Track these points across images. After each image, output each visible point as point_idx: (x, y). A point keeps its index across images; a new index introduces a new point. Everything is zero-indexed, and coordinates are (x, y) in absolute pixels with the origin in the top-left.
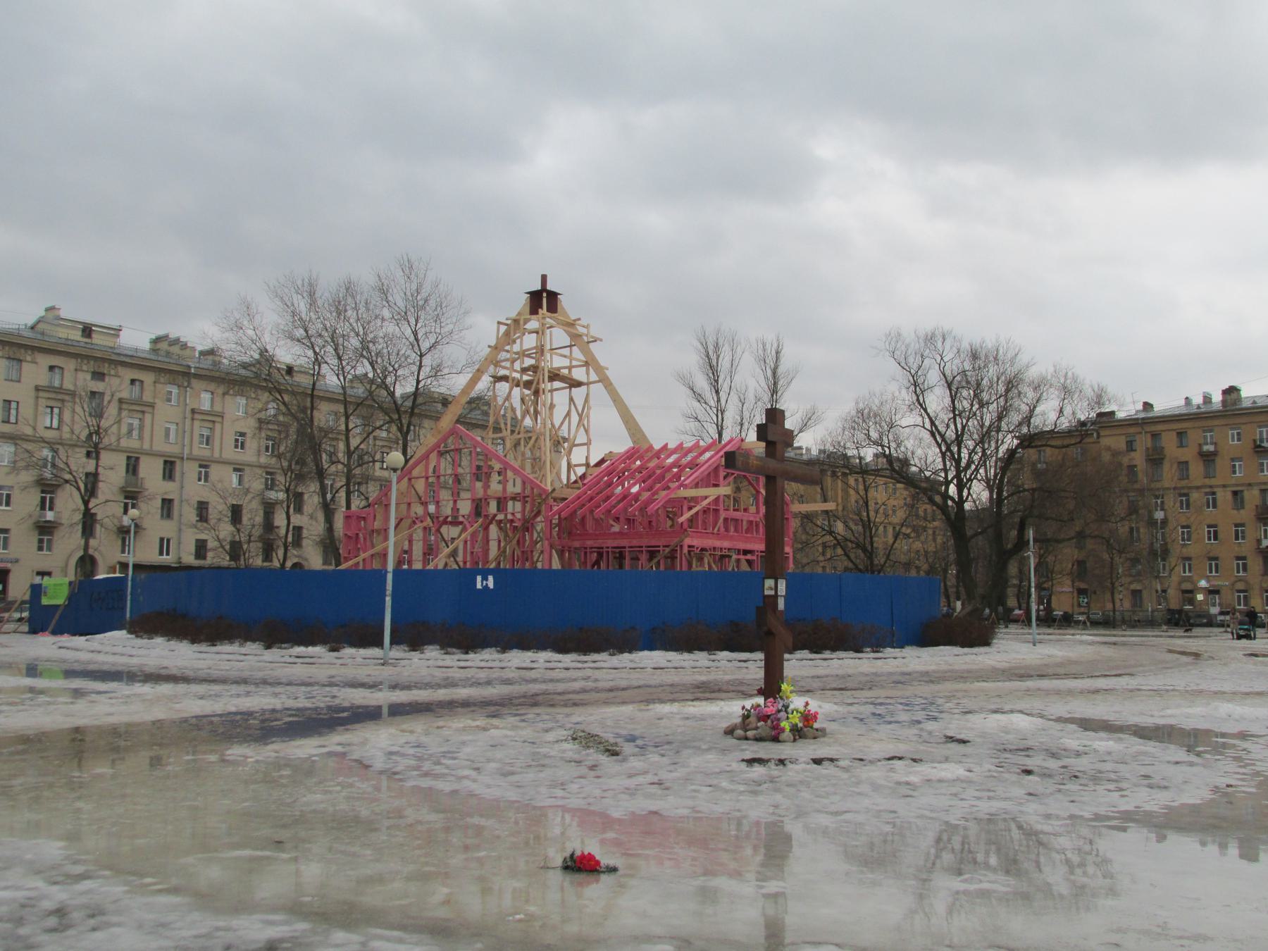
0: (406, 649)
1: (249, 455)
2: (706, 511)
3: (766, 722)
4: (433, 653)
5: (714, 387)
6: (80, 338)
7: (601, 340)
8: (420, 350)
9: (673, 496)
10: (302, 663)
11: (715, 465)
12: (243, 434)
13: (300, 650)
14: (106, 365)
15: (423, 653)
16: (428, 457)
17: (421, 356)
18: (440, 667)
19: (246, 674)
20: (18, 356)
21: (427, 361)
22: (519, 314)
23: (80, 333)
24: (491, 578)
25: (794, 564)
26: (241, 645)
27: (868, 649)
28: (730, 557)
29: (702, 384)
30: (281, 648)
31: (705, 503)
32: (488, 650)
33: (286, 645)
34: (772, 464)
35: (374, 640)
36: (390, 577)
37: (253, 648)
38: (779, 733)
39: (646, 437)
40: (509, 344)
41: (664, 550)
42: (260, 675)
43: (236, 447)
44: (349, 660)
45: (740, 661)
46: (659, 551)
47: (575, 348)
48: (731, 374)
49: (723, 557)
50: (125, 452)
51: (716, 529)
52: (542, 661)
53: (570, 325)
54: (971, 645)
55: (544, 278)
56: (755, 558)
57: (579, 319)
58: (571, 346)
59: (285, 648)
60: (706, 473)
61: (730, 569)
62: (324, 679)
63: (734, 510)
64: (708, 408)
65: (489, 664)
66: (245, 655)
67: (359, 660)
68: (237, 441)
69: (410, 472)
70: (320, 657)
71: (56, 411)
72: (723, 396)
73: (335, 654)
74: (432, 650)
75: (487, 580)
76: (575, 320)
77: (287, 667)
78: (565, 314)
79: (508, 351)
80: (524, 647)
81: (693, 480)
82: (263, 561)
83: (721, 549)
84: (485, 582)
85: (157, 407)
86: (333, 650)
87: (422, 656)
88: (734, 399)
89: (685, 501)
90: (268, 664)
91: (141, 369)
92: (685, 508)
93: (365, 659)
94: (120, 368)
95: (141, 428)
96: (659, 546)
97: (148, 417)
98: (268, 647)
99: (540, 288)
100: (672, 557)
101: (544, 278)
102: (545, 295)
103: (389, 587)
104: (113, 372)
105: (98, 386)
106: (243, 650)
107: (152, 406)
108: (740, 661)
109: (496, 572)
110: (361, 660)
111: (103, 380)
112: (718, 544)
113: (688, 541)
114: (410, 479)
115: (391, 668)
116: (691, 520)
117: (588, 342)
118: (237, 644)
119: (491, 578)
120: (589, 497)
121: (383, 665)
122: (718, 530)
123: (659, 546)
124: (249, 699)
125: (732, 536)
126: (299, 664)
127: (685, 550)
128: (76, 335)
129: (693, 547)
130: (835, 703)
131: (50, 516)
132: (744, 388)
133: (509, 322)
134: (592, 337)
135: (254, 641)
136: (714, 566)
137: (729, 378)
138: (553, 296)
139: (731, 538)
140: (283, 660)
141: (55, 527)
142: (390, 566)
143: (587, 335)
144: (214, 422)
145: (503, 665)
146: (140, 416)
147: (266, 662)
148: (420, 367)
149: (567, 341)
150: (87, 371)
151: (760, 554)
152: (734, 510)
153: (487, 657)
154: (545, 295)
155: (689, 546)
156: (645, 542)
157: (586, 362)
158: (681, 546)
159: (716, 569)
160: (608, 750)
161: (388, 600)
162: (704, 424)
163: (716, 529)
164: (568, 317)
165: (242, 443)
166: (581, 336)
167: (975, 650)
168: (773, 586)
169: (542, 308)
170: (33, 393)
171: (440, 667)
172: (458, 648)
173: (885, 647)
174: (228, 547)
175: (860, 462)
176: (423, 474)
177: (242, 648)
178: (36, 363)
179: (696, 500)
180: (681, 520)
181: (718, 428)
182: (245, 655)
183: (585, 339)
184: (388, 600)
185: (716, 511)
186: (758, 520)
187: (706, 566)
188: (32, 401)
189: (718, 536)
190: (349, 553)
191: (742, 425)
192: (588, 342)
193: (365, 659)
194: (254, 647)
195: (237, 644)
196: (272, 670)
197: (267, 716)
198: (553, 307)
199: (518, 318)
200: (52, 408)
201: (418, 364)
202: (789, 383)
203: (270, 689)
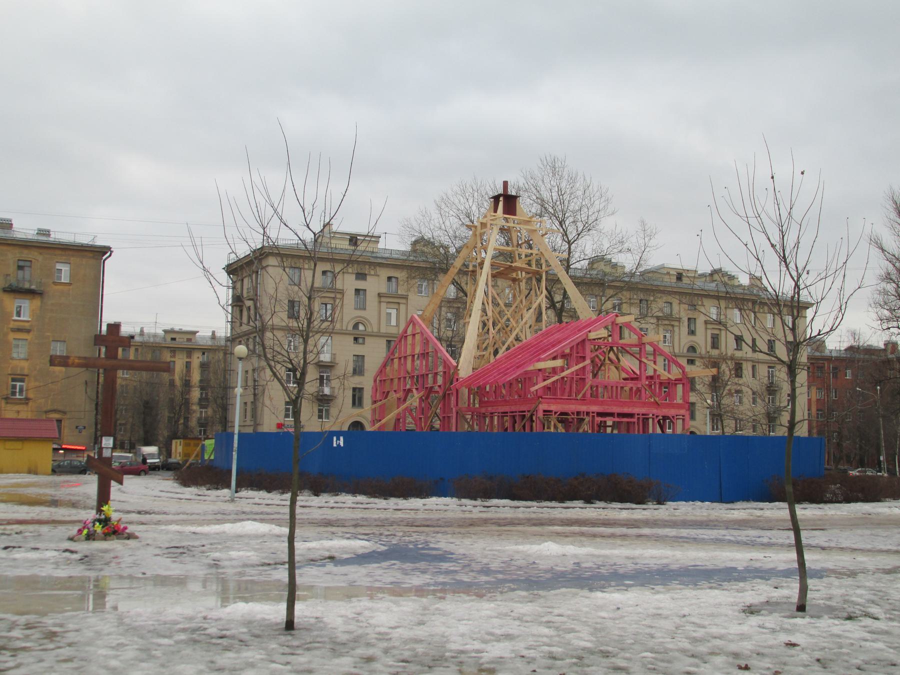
6: (347, 247)
11: (580, 339)
14: (367, 267)
17: (570, 243)
20: (298, 265)
23: (348, 243)
24: (342, 438)
36: (236, 437)
50: (767, 363)
55: (505, 184)
71: (329, 307)
85: (409, 297)
91: (396, 268)
94: (378, 268)
95: (672, 337)
96: (525, 412)
97: (403, 307)
101: (505, 184)
104: (372, 272)
105: (361, 285)
107: (406, 297)
111: (365, 279)
113: (543, 407)
119: (342, 438)
122: (584, 396)
123: (525, 412)
127: (540, 414)
128: (345, 245)
130: (219, 619)
131: (327, 391)
139: (602, 403)
141: (332, 400)
142: (236, 431)
144: (399, 303)
146: (396, 306)
150: (352, 273)
155: (544, 411)
170: (377, 299)
175: (282, 259)
178: (378, 276)
186: (639, 386)
188: (376, 304)
200: (326, 304)
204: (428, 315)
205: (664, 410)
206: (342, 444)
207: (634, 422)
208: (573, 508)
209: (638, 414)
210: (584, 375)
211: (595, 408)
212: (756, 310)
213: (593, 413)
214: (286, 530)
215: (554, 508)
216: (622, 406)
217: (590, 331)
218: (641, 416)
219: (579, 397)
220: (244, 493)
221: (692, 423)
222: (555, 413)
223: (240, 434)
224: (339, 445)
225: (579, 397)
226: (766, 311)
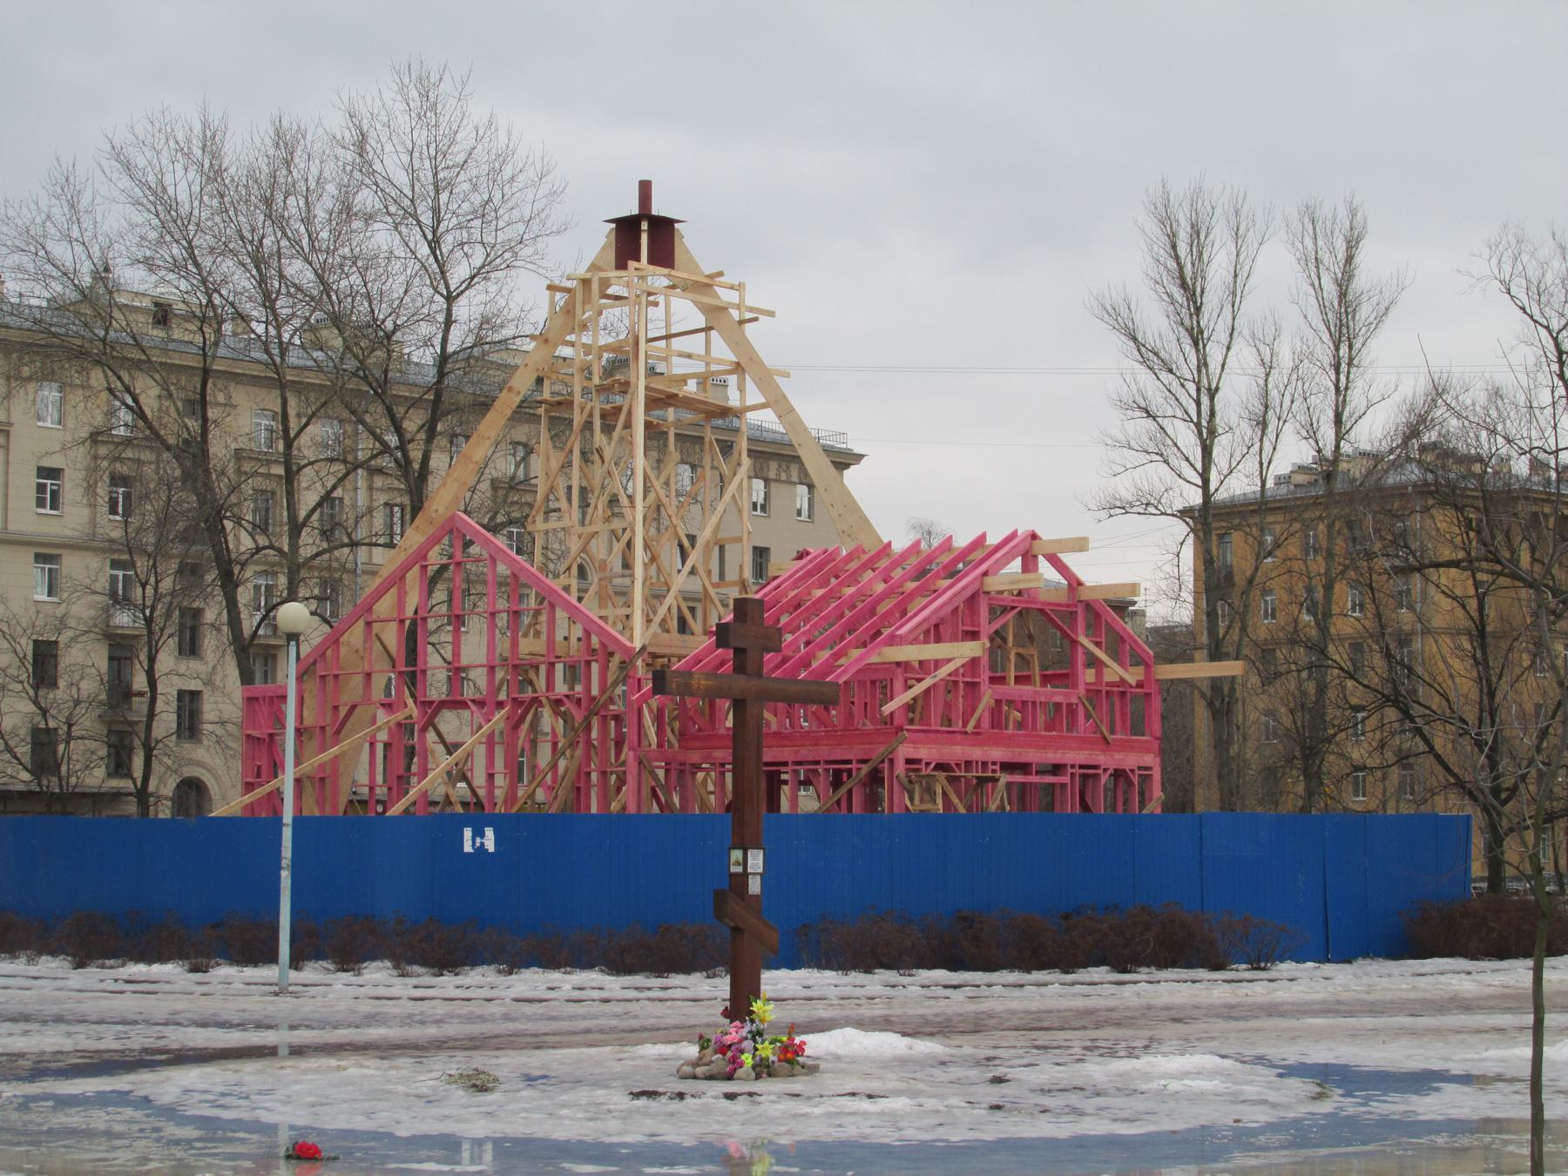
0: (331, 967)
1: (74, 517)
2: (951, 684)
3: (724, 1054)
4: (377, 974)
5: (1190, 331)
7: (771, 314)
8: (447, 287)
9: (874, 659)
10: (134, 992)
11: (969, 592)
12: (53, 473)
13: (137, 969)
15: (359, 974)
16: (403, 578)
17: (450, 299)
18: (378, 998)
19: (31, 1009)
21: (461, 310)
22: (594, 267)
24: (489, 833)
25: (1164, 789)
26: (30, 961)
27: (1244, 966)
28: (995, 780)
29: (1157, 323)
30: (103, 967)
31: (943, 672)
32: (479, 969)
33: (112, 962)
34: (741, 683)
35: (258, 951)
36: (287, 833)
37: (50, 965)
38: (735, 1070)
39: (867, 521)
40: (572, 331)
41: (859, 769)
42: (55, 1009)
43: (40, 503)
44: (220, 987)
45: (946, 987)
46: (850, 772)
47: (714, 333)
48: (1234, 295)
49: (982, 781)
51: (972, 723)
52: (567, 987)
53: (701, 287)
54: (1502, 957)
55: (645, 189)
56: (1066, 779)
57: (720, 274)
58: (707, 329)
59: (111, 967)
60: (950, 608)
61: (993, 807)
62: (161, 1017)
63: (1018, 680)
64: (1175, 386)
65: (467, 994)
66: (36, 978)
67: (238, 986)
68: (41, 488)
69: (370, 610)
70: (168, 982)
72: (1214, 353)
73: (198, 976)
74: (379, 969)
75: (482, 836)
76: (712, 276)
77: (106, 998)
78: (692, 265)
79: (572, 344)
80: (550, 961)
81: (921, 623)
82: (110, 775)
83: (984, 764)
84: (478, 840)
86: (195, 969)
87: (359, 980)
88: (1244, 357)
89: (899, 670)
90: (74, 994)
92: (898, 685)
93: (248, 984)
96: (849, 762)
98: (80, 965)
99: (635, 211)
100: (875, 778)
101: (645, 189)
102: (645, 226)
103: (287, 852)
106: (33, 970)
108: (946, 987)
109: (498, 823)
110: (241, 986)
112: (976, 753)
113: (904, 751)
114: (369, 624)
115: (289, 999)
116: (910, 707)
117: (742, 322)
118: (23, 959)
119: (489, 833)
120: (718, 662)
121: (277, 994)
122: (977, 726)
123: (849, 762)
124: (24, 1039)
125: (1010, 737)
126: (128, 994)
127: (900, 768)
129: (918, 761)
132: (1270, 331)
133: (569, 284)
134: (751, 310)
135: (54, 953)
136: (955, 800)
137: (1228, 309)
138: (663, 229)
139: (1009, 741)
140: (102, 986)
142: (288, 816)
143: (738, 307)
145: (490, 994)
147: (72, 990)
148: (449, 322)
149: (701, 322)
151: (1078, 771)
152: (1018, 680)
153: (479, 979)
154: (645, 226)
155: (909, 761)
156: (824, 753)
157: (738, 364)
158: (892, 761)
159: (962, 810)
160: (474, 1086)
161: (285, 876)
162: (1165, 422)
163: (972, 723)
164: (696, 268)
165: (55, 494)
166: (724, 309)
167: (1506, 964)
168: (741, 860)
169: (638, 259)
171: (378, 998)
172: (424, 964)
173: (1273, 962)
174: (24, 750)
176: (395, 615)
177: (30, 968)
179: (926, 667)
180: (888, 708)
181: (1200, 433)
182: (36, 978)
183: (735, 315)
184: (285, 876)
185: (973, 687)
186: (1074, 700)
187: (939, 801)
189: (977, 737)
190: (259, 775)
191: (1263, 424)
192: (742, 322)
193: (248, 984)
194: (53, 965)
195: (23, 959)
196: (79, 1002)
197: (45, 1058)
198: (664, 253)
199: (588, 276)
201: (441, 318)
202: (1380, 319)
203: (63, 1027)
204: (441, 510)
205: (1119, 756)
206: (491, 847)
207: (1063, 786)
208: (1135, 983)
209: (1073, 766)
210: (973, 676)
211: (997, 754)
212: (772, 475)
213: (994, 763)
214: (1529, 1019)
215: (422, 999)
216: (1044, 747)
217: (985, 574)
218: (1078, 771)
219: (970, 728)
220: (312, 972)
221: (189, 750)
222: (928, 764)
223: (298, 821)
224: (481, 849)
225: (970, 728)
226: (795, 478)
